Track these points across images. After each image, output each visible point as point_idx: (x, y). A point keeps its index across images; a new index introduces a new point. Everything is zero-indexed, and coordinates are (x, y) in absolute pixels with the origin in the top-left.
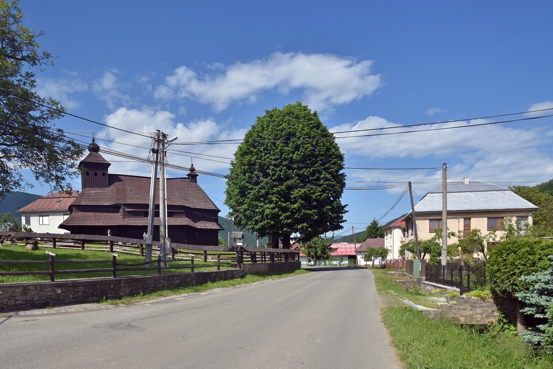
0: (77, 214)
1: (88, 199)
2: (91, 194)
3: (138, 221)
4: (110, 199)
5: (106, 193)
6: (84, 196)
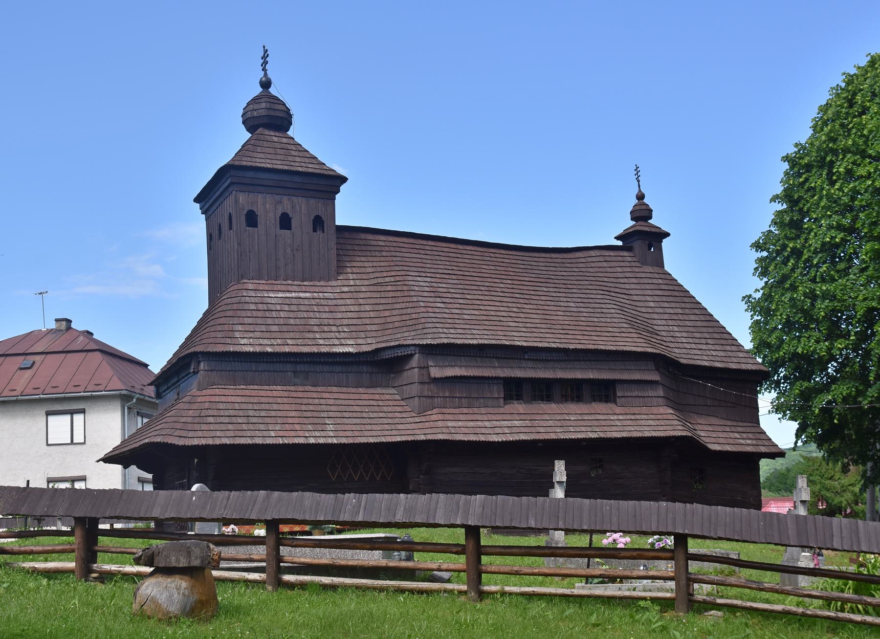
0: (217, 391)
1: (264, 328)
2: (271, 307)
3: (487, 424)
4: (353, 328)
5: (330, 302)
6: (243, 314)
